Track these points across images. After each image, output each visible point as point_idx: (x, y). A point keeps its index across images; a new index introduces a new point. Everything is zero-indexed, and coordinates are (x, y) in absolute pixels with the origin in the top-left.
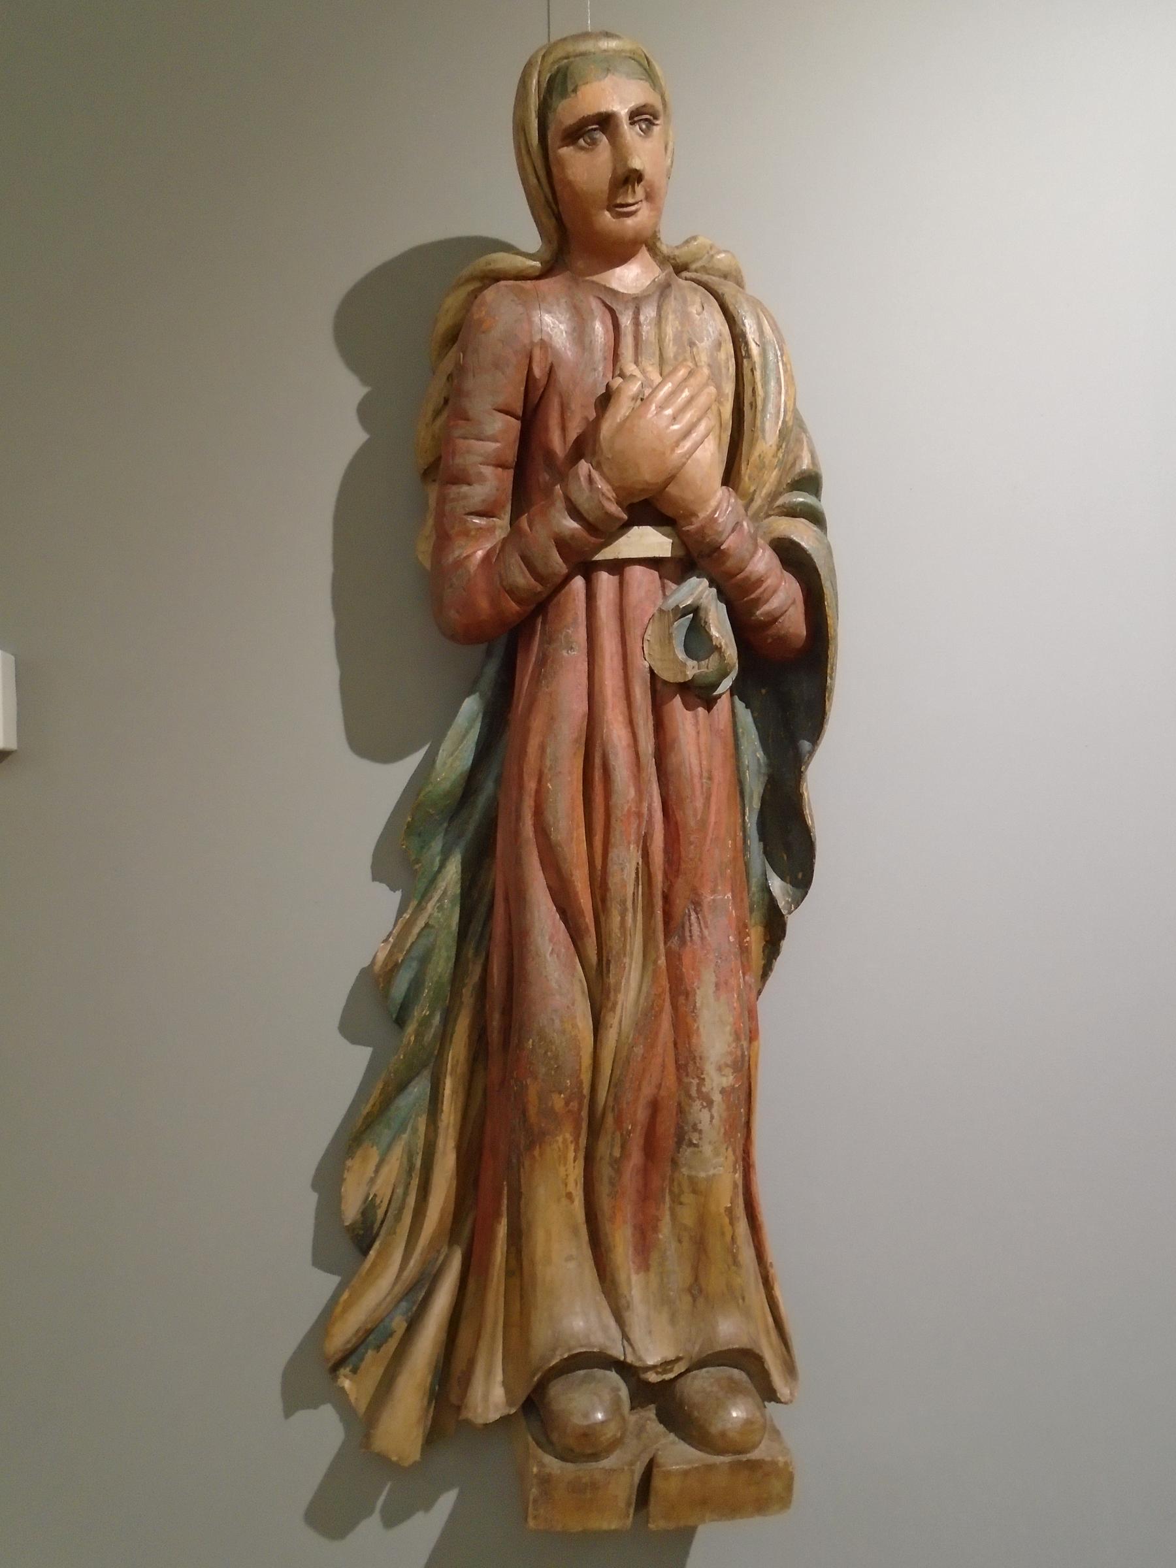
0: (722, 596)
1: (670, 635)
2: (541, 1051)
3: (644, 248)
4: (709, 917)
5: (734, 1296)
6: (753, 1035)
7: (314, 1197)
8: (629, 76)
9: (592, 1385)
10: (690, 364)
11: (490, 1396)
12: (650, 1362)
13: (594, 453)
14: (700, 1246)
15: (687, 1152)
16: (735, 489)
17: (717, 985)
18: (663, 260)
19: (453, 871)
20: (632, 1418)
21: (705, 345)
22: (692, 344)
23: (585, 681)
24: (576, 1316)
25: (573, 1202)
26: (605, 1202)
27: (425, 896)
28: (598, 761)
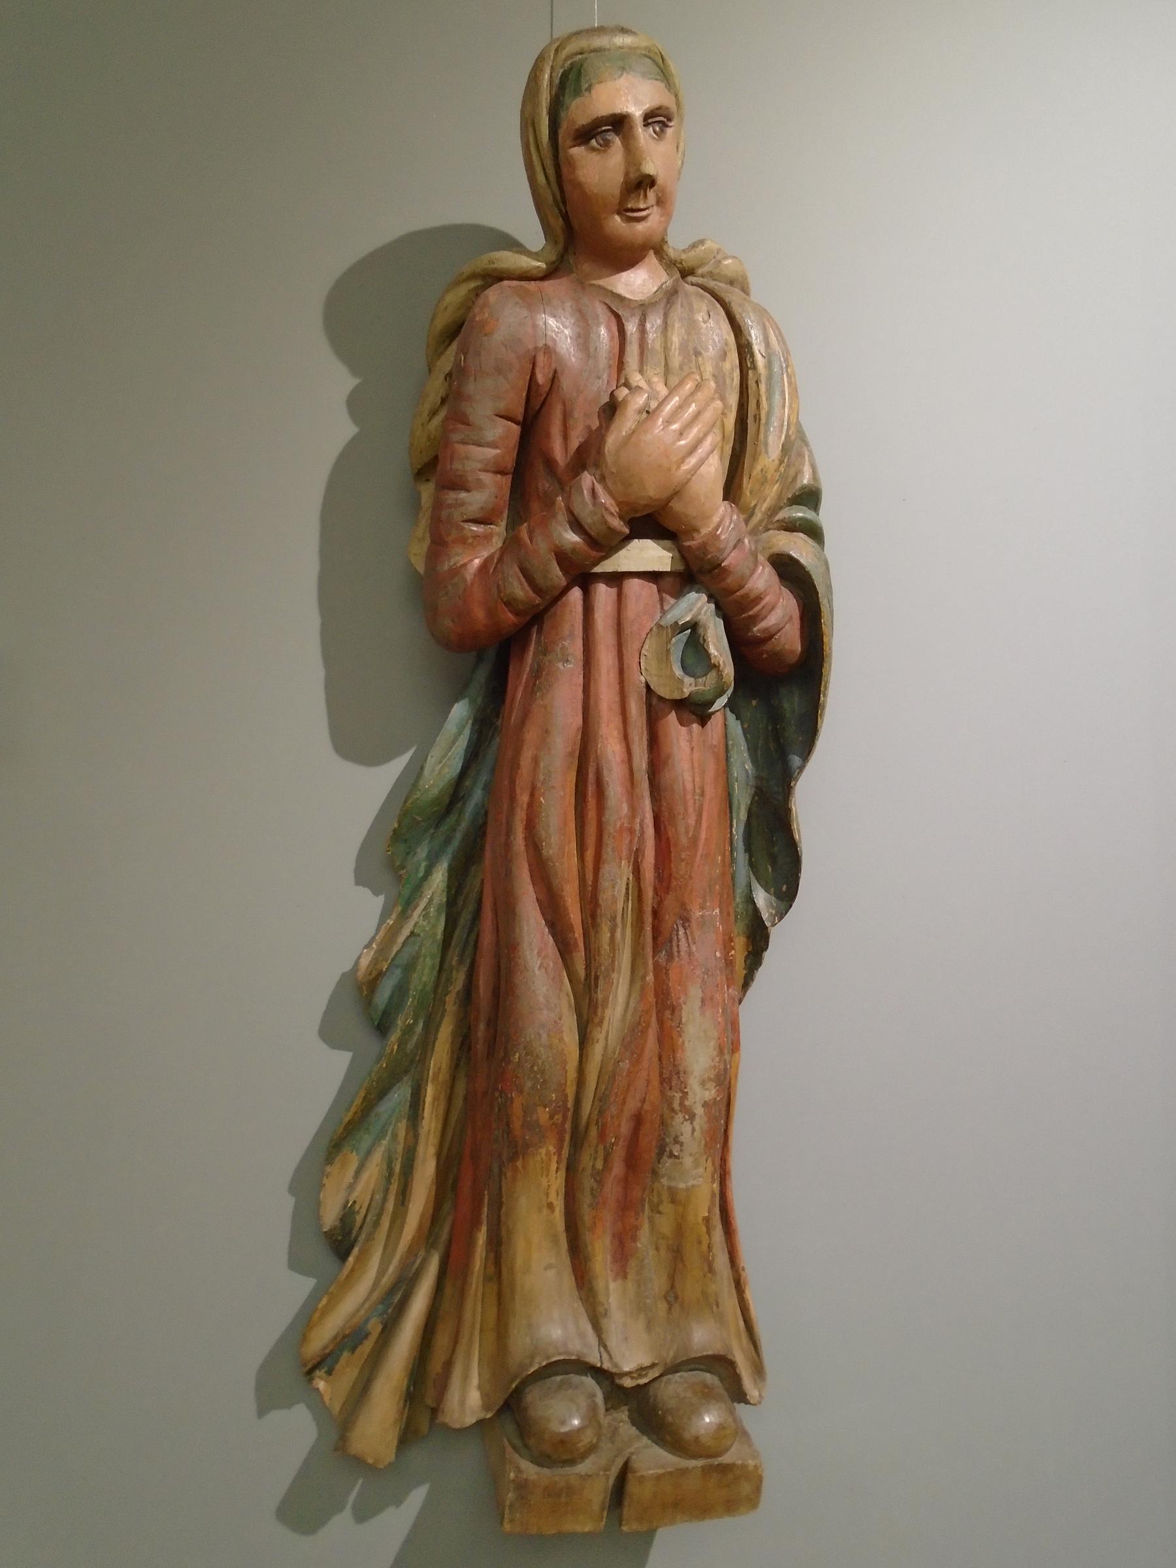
0: (720, 610)
1: (668, 651)
2: (528, 1065)
3: (651, 252)
4: (697, 933)
5: (709, 1303)
6: (735, 1047)
7: (290, 1201)
8: (644, 75)
9: (570, 1391)
10: (698, 378)
11: (468, 1400)
12: (626, 1369)
13: (597, 465)
14: (677, 1254)
15: (668, 1162)
16: (737, 505)
17: (703, 1001)
18: (670, 264)
19: (439, 878)
20: (605, 1420)
21: (711, 352)
22: (697, 354)
23: (580, 695)
24: (554, 1324)
25: (553, 1211)
26: (586, 1212)
27: (409, 904)
28: (591, 776)
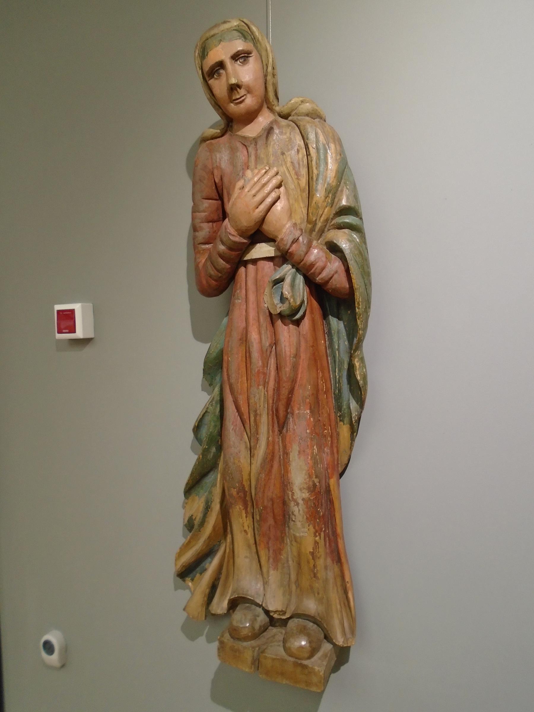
17: (299, 452)
24: (249, 583)
25: (247, 534)
